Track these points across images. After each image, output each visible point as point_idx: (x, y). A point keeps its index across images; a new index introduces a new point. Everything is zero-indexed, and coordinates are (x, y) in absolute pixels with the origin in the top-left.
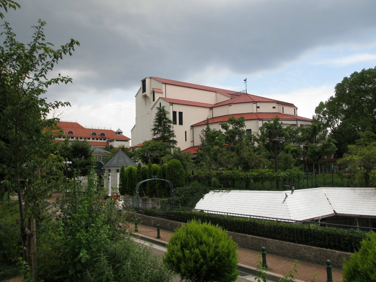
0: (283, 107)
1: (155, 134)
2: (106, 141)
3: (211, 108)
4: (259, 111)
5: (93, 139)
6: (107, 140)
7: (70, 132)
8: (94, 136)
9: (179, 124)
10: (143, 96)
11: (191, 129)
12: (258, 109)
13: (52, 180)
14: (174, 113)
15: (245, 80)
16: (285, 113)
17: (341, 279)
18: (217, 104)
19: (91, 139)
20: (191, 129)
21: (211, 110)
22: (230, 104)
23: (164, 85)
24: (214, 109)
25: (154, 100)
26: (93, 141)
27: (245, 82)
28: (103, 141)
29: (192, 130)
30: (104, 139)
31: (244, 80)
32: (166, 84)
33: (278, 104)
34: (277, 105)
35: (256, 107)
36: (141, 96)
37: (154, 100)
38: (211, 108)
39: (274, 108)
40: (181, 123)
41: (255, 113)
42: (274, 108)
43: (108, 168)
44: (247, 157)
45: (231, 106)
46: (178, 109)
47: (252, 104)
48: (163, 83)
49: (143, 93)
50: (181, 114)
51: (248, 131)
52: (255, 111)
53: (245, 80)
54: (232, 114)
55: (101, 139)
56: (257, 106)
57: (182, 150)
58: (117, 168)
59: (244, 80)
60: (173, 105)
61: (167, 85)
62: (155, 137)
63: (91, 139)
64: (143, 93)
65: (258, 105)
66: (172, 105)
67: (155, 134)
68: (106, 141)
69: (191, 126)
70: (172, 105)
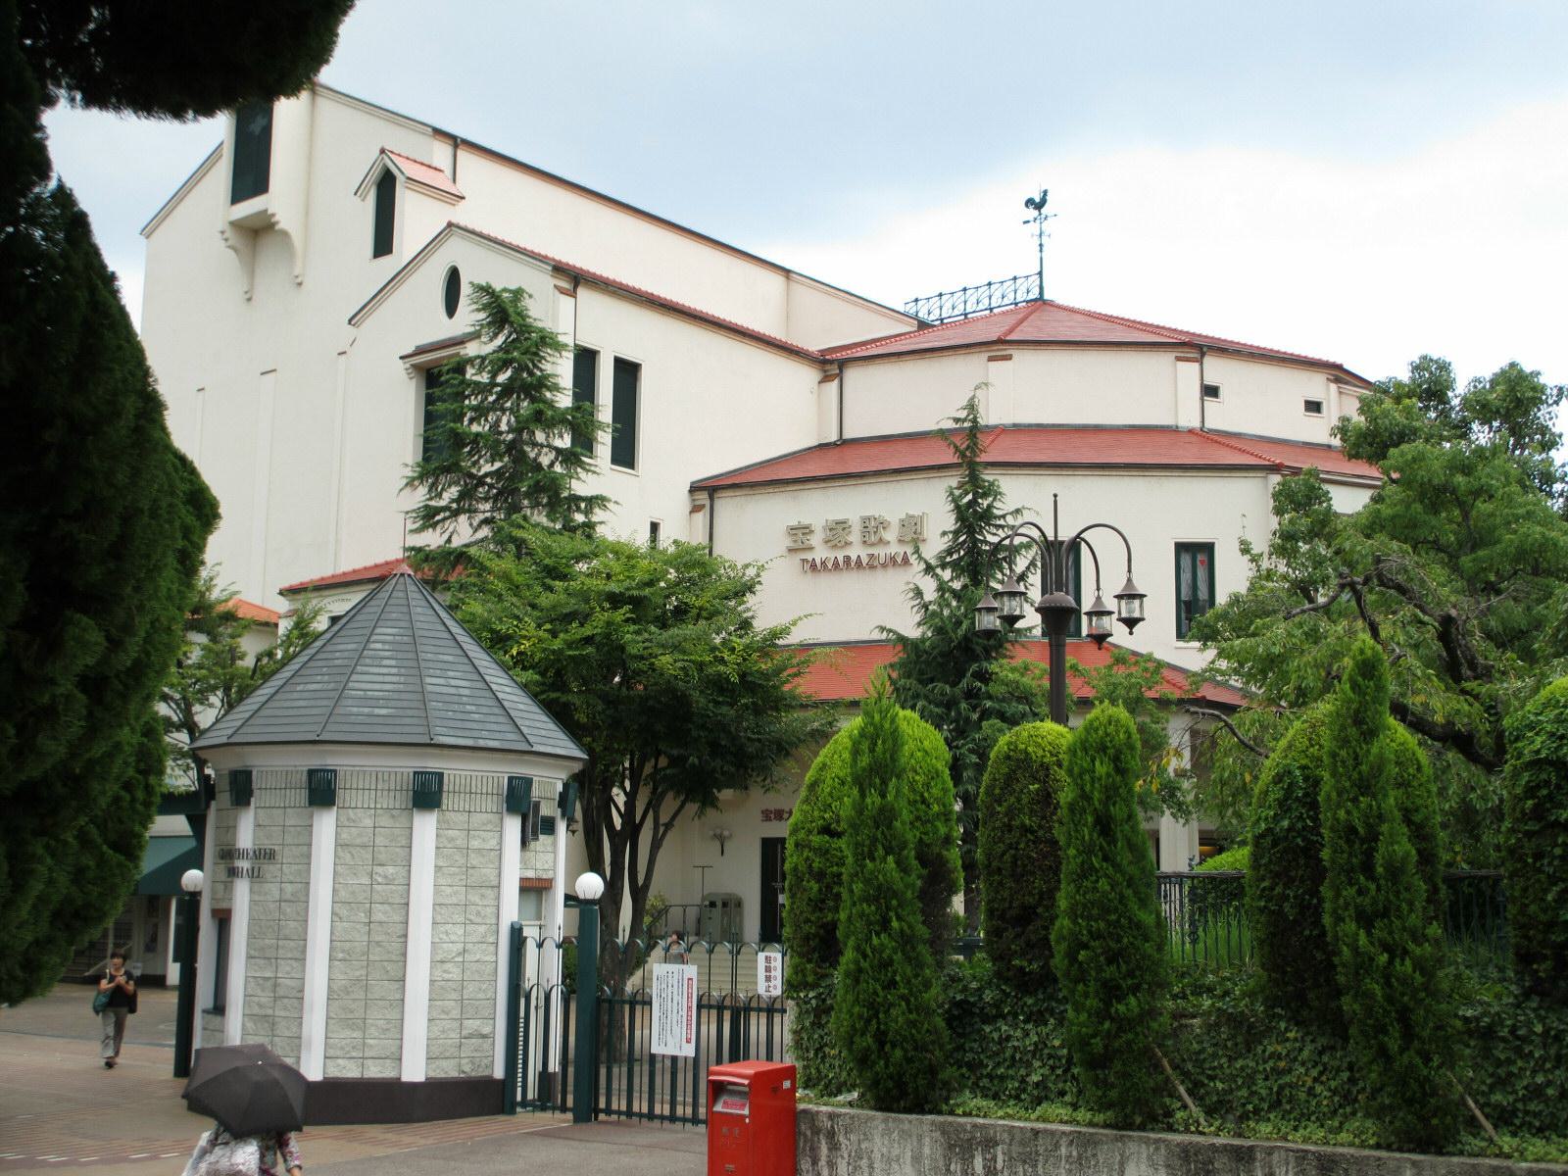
1: (429, 517)
3: (832, 365)
9: (614, 461)
10: (237, 225)
11: (696, 509)
12: (1210, 402)
14: (586, 359)
15: (1038, 205)
20: (696, 509)
21: (835, 384)
24: (854, 376)
25: (383, 243)
27: (1032, 213)
29: (701, 518)
31: (1030, 202)
33: (1337, 380)
34: (1333, 387)
36: (221, 223)
37: (383, 243)
39: (1313, 407)
40: (625, 454)
42: (1313, 407)
43: (306, 761)
45: (1008, 358)
46: (612, 331)
47: (1164, 361)
49: (238, 195)
50: (627, 372)
51: (1186, 560)
52: (1189, 419)
53: (1038, 205)
54: (1008, 420)
57: (1244, 591)
58: (408, 765)
59: (1030, 202)
60: (582, 292)
61: (463, 155)
62: (432, 539)
64: (238, 195)
65: (1216, 370)
66: (573, 294)
67: (429, 517)
69: (695, 488)
70: (573, 294)
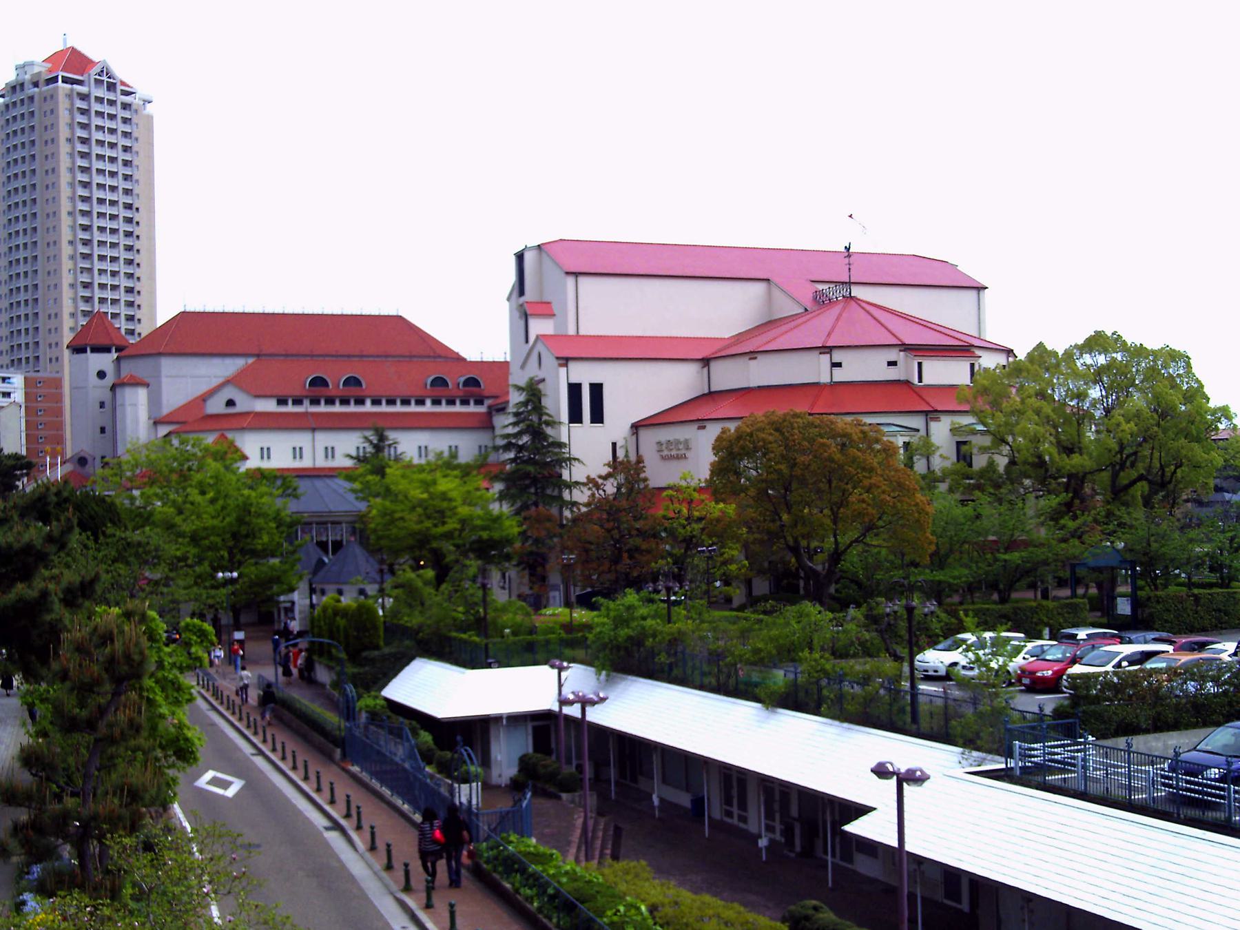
0: (920, 364)
2: (482, 409)
4: (840, 375)
5: (436, 402)
6: (487, 402)
7: (353, 382)
8: (439, 391)
12: (836, 370)
13: (1030, 413)
14: (574, 390)
16: (927, 380)
17: (7, 451)
18: (770, 324)
19: (428, 402)
22: (753, 355)
23: (570, 281)
26: (437, 409)
28: (472, 408)
30: (479, 402)
32: (576, 274)
35: (828, 365)
38: (706, 362)
39: (892, 364)
40: (598, 417)
41: (825, 385)
42: (892, 364)
44: (1226, 478)
46: (584, 374)
48: (567, 273)
50: (597, 390)
52: (825, 379)
54: (756, 385)
55: (465, 402)
56: (835, 361)
63: (428, 402)
65: (838, 356)
68: (482, 409)
